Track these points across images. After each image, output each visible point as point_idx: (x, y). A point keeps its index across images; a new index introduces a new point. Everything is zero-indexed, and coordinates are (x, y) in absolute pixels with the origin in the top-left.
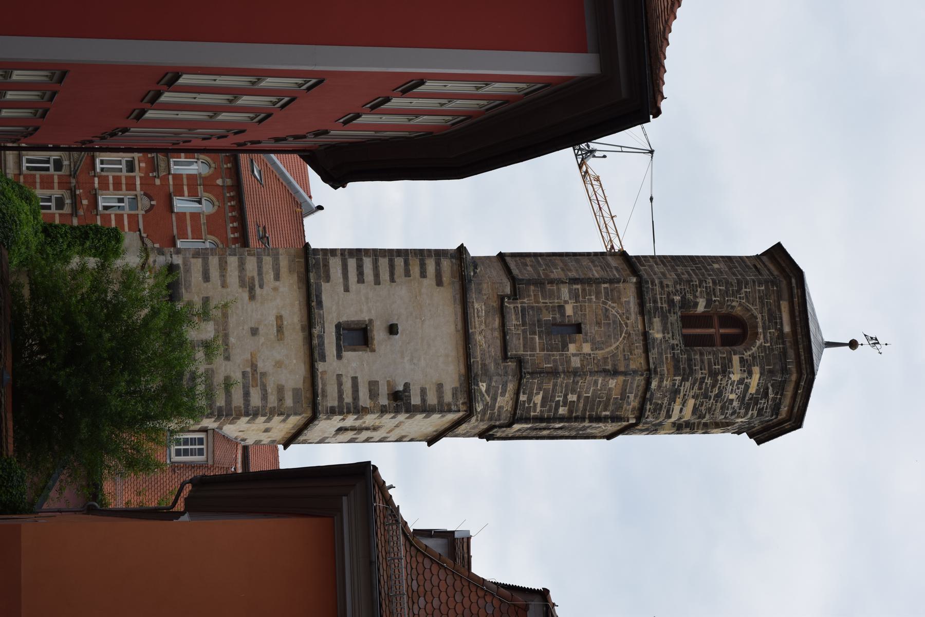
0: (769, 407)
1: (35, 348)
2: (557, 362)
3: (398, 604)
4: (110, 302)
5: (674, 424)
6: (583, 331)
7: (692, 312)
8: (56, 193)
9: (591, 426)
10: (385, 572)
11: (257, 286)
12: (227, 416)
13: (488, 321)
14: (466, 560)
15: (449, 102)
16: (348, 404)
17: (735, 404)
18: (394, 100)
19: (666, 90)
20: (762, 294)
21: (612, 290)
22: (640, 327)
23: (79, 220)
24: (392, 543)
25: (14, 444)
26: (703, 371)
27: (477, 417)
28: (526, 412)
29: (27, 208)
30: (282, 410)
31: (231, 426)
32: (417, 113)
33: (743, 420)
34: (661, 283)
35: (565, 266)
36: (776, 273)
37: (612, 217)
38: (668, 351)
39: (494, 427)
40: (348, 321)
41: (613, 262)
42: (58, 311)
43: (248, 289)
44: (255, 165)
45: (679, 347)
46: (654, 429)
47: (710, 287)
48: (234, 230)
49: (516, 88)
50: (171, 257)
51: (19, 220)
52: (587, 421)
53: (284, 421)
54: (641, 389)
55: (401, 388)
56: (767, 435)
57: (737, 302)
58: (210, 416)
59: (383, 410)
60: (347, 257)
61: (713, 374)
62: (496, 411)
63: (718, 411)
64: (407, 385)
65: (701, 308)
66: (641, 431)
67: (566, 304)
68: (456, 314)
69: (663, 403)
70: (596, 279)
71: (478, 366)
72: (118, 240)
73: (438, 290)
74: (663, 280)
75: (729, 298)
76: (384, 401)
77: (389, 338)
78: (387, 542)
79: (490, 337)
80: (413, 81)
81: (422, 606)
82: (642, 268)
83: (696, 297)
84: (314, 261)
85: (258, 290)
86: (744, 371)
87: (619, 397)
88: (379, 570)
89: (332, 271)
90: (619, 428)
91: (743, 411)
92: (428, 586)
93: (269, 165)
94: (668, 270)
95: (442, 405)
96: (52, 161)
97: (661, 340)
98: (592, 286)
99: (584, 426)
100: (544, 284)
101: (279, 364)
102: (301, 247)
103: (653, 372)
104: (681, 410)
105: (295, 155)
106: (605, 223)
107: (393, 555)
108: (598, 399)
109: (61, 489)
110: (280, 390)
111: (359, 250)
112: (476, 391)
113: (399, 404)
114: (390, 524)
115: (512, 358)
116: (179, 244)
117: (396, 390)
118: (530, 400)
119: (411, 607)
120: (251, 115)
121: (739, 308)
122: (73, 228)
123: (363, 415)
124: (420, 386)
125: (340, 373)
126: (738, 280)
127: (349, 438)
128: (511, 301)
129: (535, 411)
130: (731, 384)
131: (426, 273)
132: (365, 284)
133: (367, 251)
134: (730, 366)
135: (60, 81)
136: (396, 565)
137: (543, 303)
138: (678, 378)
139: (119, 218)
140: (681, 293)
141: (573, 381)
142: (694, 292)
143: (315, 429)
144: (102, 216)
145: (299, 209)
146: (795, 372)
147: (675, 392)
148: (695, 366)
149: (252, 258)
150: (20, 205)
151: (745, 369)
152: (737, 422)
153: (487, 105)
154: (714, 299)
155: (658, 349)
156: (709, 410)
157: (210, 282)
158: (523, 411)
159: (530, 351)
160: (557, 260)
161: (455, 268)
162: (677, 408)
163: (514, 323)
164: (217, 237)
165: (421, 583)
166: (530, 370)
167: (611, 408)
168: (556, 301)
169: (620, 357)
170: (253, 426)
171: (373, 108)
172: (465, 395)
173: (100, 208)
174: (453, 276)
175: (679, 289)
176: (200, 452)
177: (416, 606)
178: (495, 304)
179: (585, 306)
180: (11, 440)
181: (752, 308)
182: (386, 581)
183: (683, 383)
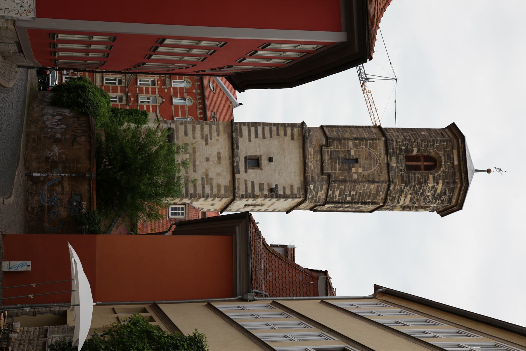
0: (446, 199)
1: (107, 163)
2: (346, 176)
3: (260, 274)
4: (141, 143)
5: (401, 206)
6: (359, 162)
7: (410, 154)
8: (119, 95)
9: (362, 206)
10: (254, 260)
11: (209, 138)
12: (194, 197)
13: (314, 157)
14: (292, 258)
15: (284, 53)
16: (249, 193)
17: (430, 197)
18: (259, 52)
19: (375, 48)
20: (444, 146)
21: (373, 144)
22: (386, 161)
23: (129, 107)
24: (258, 247)
25: (96, 205)
26: (415, 182)
27: (309, 201)
28: (332, 199)
29: (104, 100)
30: (220, 196)
31: (196, 202)
32: (271, 58)
33: (434, 205)
34: (396, 141)
35: (351, 132)
36: (452, 136)
37: (376, 110)
38: (399, 172)
39: (317, 206)
40: (250, 156)
41: (374, 131)
42: (117, 146)
43: (205, 140)
44: (211, 83)
45: (404, 171)
46: (392, 209)
47: (419, 143)
48: (200, 113)
49: (312, 47)
50: (170, 125)
51: (100, 105)
52: (360, 204)
53: (220, 200)
54: (386, 189)
55: (274, 187)
56: (446, 213)
57: (432, 150)
58: (187, 197)
59: (266, 197)
60: (250, 126)
61: (420, 183)
62: (318, 198)
63: (422, 200)
64: (277, 186)
65: (415, 153)
66: (386, 209)
67: (351, 149)
68: (300, 153)
69: (396, 197)
70: (366, 138)
71: (310, 177)
72: (146, 116)
73: (292, 142)
74: (397, 139)
75: (428, 148)
76: (266, 192)
77: (269, 164)
78: (255, 247)
79: (315, 164)
80: (266, 43)
81: (271, 276)
82: (387, 133)
83: (412, 147)
84: (235, 128)
85: (209, 140)
86: (435, 182)
87: (375, 193)
88: (251, 258)
89: (243, 132)
90: (375, 208)
91: (434, 201)
92: (273, 267)
93: (217, 84)
94: (400, 134)
95: (292, 195)
96: (117, 80)
97: (396, 167)
98: (364, 142)
99: (359, 206)
100: (341, 140)
101: (218, 174)
102: (230, 120)
103: (391, 182)
104: (404, 200)
105: (223, 77)
106: (373, 113)
107: (258, 253)
108: (365, 194)
109: (117, 226)
110: (219, 186)
111: (256, 123)
112: (308, 189)
113: (273, 194)
114: (257, 239)
115: (325, 174)
116: (175, 119)
117: (272, 187)
118: (333, 193)
119: (266, 276)
120: (198, 58)
121: (433, 153)
122: (126, 110)
123: (256, 199)
124: (283, 186)
125: (246, 179)
126: (433, 140)
127: (250, 209)
128: (326, 148)
129: (336, 199)
130: (428, 188)
131: (286, 134)
132: (259, 139)
133: (259, 124)
134: (428, 180)
135: (114, 41)
136: (259, 257)
137: (341, 149)
138: (403, 185)
139: (148, 107)
140: (406, 145)
141: (354, 185)
142: (412, 145)
143: (235, 204)
144: (140, 106)
145: (231, 105)
146: (459, 183)
147: (402, 191)
148: (411, 179)
149: (207, 126)
150: (101, 99)
151: (435, 181)
152: (431, 206)
153: (300, 55)
154: (421, 148)
155: (394, 171)
156: (418, 200)
157: (188, 137)
158: (330, 198)
159: (334, 171)
160: (348, 129)
161: (300, 132)
162: (402, 199)
163: (326, 158)
164: (193, 116)
165: (271, 266)
166: (334, 180)
167: (371, 198)
168: (347, 148)
169: (376, 174)
170: (206, 203)
171: (250, 55)
172: (303, 191)
173: (139, 102)
174: (299, 136)
175: (405, 144)
176: (182, 214)
177: (268, 276)
178: (318, 149)
179: (360, 151)
180: (95, 204)
181: (440, 153)
182: (254, 263)
183: (406, 187)
